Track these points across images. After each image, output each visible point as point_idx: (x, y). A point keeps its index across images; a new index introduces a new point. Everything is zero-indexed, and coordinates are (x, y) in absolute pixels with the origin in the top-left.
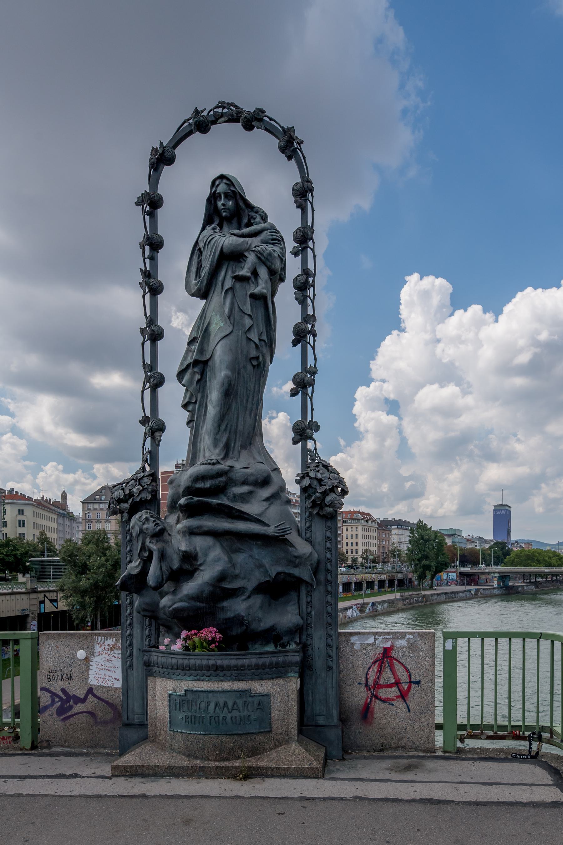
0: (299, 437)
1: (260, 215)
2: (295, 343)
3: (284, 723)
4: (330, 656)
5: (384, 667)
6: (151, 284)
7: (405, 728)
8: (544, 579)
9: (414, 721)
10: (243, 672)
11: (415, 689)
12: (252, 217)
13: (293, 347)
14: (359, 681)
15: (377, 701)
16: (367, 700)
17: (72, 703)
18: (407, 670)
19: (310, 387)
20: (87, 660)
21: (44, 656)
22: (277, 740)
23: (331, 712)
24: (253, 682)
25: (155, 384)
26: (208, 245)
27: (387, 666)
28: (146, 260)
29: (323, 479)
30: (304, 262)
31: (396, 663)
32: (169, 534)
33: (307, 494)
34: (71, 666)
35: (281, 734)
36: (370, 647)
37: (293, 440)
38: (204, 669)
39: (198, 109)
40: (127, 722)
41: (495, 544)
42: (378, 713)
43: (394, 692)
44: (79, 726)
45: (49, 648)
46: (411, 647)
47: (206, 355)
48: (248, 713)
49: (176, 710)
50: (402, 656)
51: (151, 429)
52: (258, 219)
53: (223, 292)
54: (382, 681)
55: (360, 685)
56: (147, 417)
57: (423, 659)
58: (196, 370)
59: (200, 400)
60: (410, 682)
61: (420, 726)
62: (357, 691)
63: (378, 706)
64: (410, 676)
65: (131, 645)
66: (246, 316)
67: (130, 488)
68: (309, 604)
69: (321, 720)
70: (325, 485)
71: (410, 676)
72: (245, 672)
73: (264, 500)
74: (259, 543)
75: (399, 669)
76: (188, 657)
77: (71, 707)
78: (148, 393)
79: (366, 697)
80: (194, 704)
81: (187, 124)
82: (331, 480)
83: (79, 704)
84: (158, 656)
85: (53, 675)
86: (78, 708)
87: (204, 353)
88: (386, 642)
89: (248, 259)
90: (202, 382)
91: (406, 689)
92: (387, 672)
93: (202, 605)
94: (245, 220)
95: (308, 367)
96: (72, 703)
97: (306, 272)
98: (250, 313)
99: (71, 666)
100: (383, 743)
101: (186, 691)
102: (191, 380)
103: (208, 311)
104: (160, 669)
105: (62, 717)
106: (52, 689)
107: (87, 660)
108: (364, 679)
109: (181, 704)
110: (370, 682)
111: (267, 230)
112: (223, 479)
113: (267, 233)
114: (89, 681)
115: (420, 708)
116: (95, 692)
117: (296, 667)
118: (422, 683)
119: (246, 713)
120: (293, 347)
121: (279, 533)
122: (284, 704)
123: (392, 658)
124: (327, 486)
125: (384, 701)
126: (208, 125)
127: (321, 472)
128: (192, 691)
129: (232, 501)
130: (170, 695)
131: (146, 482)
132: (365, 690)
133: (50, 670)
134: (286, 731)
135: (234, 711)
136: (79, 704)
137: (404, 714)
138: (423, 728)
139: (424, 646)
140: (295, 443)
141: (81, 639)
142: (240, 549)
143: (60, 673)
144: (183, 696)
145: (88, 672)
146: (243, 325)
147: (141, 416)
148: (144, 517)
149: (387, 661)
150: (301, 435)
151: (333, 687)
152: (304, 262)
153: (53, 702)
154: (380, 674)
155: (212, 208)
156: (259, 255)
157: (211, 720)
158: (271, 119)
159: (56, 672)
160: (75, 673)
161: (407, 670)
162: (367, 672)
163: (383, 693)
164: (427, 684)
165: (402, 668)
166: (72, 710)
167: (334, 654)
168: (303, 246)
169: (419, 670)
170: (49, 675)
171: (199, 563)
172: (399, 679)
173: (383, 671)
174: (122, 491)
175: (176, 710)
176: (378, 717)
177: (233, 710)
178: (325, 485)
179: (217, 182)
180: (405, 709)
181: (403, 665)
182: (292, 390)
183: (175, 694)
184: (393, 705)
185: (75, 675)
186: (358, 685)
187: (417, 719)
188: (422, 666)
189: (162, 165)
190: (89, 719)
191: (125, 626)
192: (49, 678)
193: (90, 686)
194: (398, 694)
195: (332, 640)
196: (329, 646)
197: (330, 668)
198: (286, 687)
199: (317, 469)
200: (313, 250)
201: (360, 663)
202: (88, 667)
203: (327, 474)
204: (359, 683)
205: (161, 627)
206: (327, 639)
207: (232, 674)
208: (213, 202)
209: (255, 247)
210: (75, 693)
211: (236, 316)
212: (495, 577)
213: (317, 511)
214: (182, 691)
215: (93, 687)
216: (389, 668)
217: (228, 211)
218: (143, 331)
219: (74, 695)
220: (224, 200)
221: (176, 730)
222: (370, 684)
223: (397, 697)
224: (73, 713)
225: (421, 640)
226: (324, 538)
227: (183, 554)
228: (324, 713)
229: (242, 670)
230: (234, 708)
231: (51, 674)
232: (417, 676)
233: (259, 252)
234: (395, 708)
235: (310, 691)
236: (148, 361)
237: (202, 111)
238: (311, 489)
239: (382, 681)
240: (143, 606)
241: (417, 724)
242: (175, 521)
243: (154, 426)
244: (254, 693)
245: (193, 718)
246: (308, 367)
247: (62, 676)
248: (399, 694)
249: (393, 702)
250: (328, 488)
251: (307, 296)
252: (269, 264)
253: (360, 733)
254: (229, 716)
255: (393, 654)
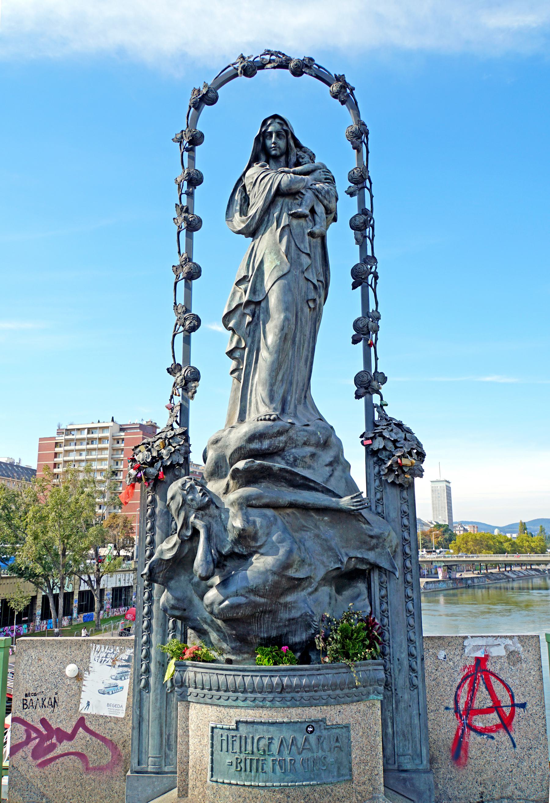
0: (363, 390)
1: (308, 155)
2: (354, 287)
3: (367, 768)
4: (413, 670)
5: (478, 684)
6: (190, 220)
7: (510, 770)
8: (497, 570)
9: (521, 760)
10: (316, 694)
11: (521, 715)
12: (300, 156)
13: (353, 289)
14: (446, 705)
15: (472, 733)
16: (458, 732)
17: (54, 740)
18: (508, 689)
19: (373, 334)
20: (79, 677)
21: (21, 672)
22: (359, 793)
23: (419, 750)
24: (329, 708)
25: (191, 327)
26: (261, 182)
27: (481, 682)
28: (182, 195)
29: (399, 440)
30: (361, 202)
31: (493, 679)
32: (217, 507)
33: (375, 459)
34: (56, 687)
35: (364, 783)
36: (458, 658)
37: (356, 393)
38: (265, 689)
39: (244, 55)
40: (138, 768)
41: (435, 526)
42: (474, 750)
43: (493, 719)
44: (63, 774)
45: (28, 660)
46: (511, 656)
47: (259, 295)
48: (324, 753)
49: (221, 751)
50: (501, 669)
51: (185, 378)
52: (307, 159)
53: (279, 230)
54: (477, 705)
55: (448, 711)
56: (179, 364)
57: (527, 672)
58: (247, 311)
59: (251, 345)
60: (513, 705)
61: (530, 767)
62: (444, 720)
63: (473, 738)
64: (512, 697)
65: (148, 656)
66: (304, 255)
67: (157, 448)
68: (383, 600)
69: (406, 761)
70: (401, 447)
71: (512, 697)
72: (318, 694)
73: (326, 465)
74: (326, 518)
75: (498, 688)
76: (241, 673)
77: (53, 747)
78: (180, 338)
79: (456, 727)
80: (249, 741)
81: (231, 68)
82: (409, 441)
83: (65, 741)
84: (195, 673)
85: (31, 700)
86: (64, 747)
87: (257, 293)
88: (478, 650)
89: (306, 196)
90: (254, 326)
91: (508, 715)
92: (482, 692)
93: (262, 600)
94: (293, 159)
95: (371, 311)
96: (54, 740)
97: (364, 212)
98: (308, 252)
99: (56, 687)
100: (482, 793)
101: (237, 722)
102: (239, 324)
103: (259, 248)
104: (214, 692)
105: (40, 761)
106: (28, 720)
107: (79, 677)
108: (452, 702)
109: (230, 742)
110: (461, 707)
111: (320, 169)
112: (283, 438)
113: (320, 172)
114: (80, 709)
115: (529, 741)
116: (88, 724)
117: (380, 685)
118: (529, 706)
119: (320, 754)
120: (353, 289)
121: (357, 506)
122: (366, 740)
123: (488, 673)
124: (404, 448)
125: (480, 732)
126: (254, 70)
127: (394, 431)
128: (246, 722)
129: (292, 466)
130: (213, 728)
131: (179, 442)
132: (455, 717)
133: (27, 693)
134: (369, 779)
135: (304, 751)
136: (65, 741)
137: (508, 750)
138: (534, 769)
139: (527, 655)
140: (358, 396)
141: (73, 649)
142: (304, 526)
143: (40, 697)
144: (233, 730)
145: (80, 696)
146: (301, 265)
147: (169, 363)
148: (188, 485)
149: (481, 676)
150: (366, 388)
151: (420, 714)
152: (361, 202)
153: (29, 739)
154: (473, 694)
155: (260, 147)
156: (317, 193)
157: (273, 764)
158: (319, 67)
159: (35, 695)
160: (62, 698)
161: (508, 689)
162: (456, 692)
163: (479, 722)
164: (535, 708)
165: (502, 686)
166: (54, 751)
167: (418, 668)
168: (360, 186)
169: (523, 689)
170: (26, 700)
171: (258, 544)
172: (499, 702)
173: (477, 690)
174: (149, 453)
175: (221, 751)
176: (474, 755)
177: (303, 749)
178: (401, 447)
179: (269, 122)
180: (509, 744)
181: (502, 681)
182: (353, 337)
183: (221, 726)
184: (492, 738)
185: (61, 699)
186: (445, 711)
187: (526, 757)
188: (526, 682)
189: (203, 104)
190: (78, 763)
191: (141, 629)
192: (26, 704)
193: (80, 716)
194: (498, 723)
195: (415, 647)
196: (411, 655)
197: (414, 686)
198: (368, 715)
199: (390, 428)
200: (370, 190)
201: (446, 679)
202: (80, 689)
203: (402, 435)
204: (447, 708)
205: (190, 631)
206: (409, 646)
207: (302, 697)
208: (261, 141)
209: (311, 185)
210: (60, 726)
211: (293, 255)
212: (440, 567)
213: (393, 479)
214: (231, 722)
215: (85, 717)
216: (484, 685)
217: (278, 149)
218: (176, 269)
219: (58, 729)
220: (275, 139)
221: (221, 781)
222: (461, 709)
223: (498, 726)
224: (56, 755)
225: (523, 647)
226: (400, 513)
227: (240, 532)
228: (410, 752)
229: (316, 691)
230: (305, 747)
231: (29, 698)
232: (522, 697)
233: (317, 190)
234: (496, 743)
235: (389, 720)
236: (181, 301)
237: (249, 57)
238: (384, 452)
239: (477, 705)
240: (172, 602)
241: (525, 764)
242: (222, 491)
243: (189, 374)
244: (330, 724)
245: (248, 762)
246: (371, 311)
247: (43, 700)
248: (499, 721)
249: (492, 734)
250: (406, 450)
251: (366, 237)
252: (326, 202)
253: (451, 779)
254: (299, 758)
255: (489, 666)
